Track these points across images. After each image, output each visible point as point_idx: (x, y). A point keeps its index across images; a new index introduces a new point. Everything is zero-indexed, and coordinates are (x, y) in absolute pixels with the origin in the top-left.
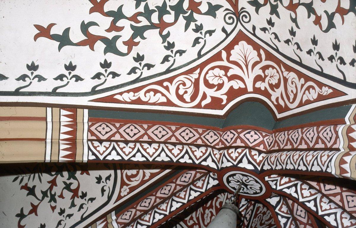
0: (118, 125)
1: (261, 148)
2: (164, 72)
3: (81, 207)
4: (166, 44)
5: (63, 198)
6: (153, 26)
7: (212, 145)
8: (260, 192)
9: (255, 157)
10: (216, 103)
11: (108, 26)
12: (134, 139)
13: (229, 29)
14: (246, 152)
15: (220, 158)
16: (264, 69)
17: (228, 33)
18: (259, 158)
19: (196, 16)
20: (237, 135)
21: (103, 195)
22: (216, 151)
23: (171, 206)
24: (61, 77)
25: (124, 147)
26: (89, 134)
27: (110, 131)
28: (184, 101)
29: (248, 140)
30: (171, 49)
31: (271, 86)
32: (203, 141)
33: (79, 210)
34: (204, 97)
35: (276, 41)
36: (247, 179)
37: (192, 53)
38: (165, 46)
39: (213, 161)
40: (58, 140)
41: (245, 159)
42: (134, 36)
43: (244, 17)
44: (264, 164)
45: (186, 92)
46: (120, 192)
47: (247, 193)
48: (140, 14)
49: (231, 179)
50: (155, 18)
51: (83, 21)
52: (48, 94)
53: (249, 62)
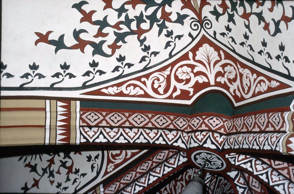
0: (104, 114)
1: (222, 131)
3: (75, 181)
4: (143, 47)
5: (60, 174)
6: (132, 32)
7: (182, 129)
9: (217, 139)
10: (185, 95)
11: (95, 33)
13: (194, 34)
15: (188, 140)
16: (224, 66)
17: (194, 37)
18: (220, 140)
19: (167, 23)
21: (92, 171)
22: (185, 134)
24: (57, 75)
25: (110, 132)
26: (81, 121)
29: (211, 124)
30: (147, 51)
31: (229, 80)
32: (174, 126)
34: (175, 89)
35: (233, 44)
37: (164, 54)
38: (142, 49)
41: (209, 140)
42: (116, 41)
43: (206, 25)
44: (224, 145)
45: (160, 86)
46: (107, 168)
47: (211, 168)
48: (121, 23)
49: (197, 157)
50: (134, 26)
51: (75, 29)
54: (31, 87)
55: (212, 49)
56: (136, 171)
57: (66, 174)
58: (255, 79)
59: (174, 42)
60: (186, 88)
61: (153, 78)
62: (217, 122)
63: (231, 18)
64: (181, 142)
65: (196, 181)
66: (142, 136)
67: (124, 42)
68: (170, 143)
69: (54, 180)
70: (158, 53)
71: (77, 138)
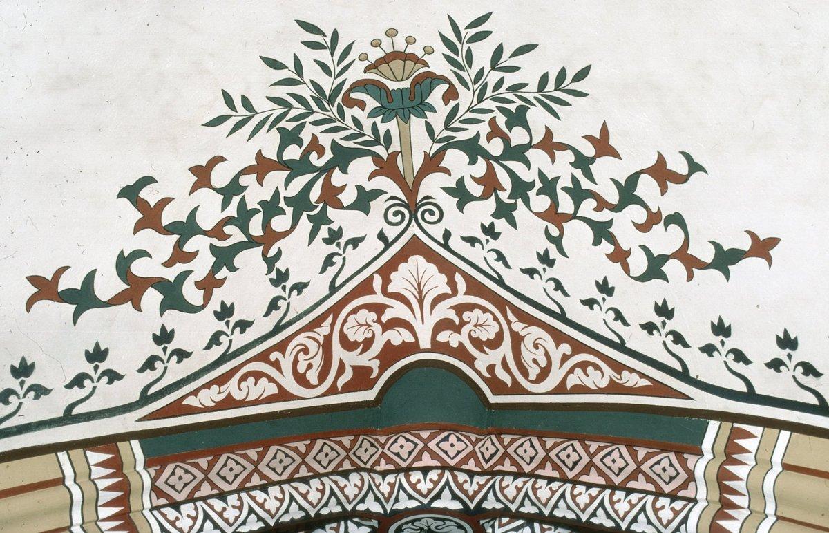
1: (471, 466)
4: (273, 275)
6: (252, 242)
7: (368, 466)
9: (466, 486)
10: (362, 378)
11: (167, 254)
13: (391, 233)
14: (448, 479)
15: (391, 494)
16: (460, 309)
17: (390, 241)
19: (331, 212)
24: (78, 381)
29: (446, 452)
32: (353, 463)
37: (319, 287)
38: (271, 280)
39: (377, 499)
42: (215, 269)
45: (310, 366)
48: (229, 221)
51: (122, 252)
53: (426, 294)
54: (17, 425)
55: (433, 268)
58: (564, 354)
59: (343, 256)
61: (294, 348)
63: (504, 211)
66: (294, 503)
67: (233, 269)
68: (349, 508)
70: (305, 285)
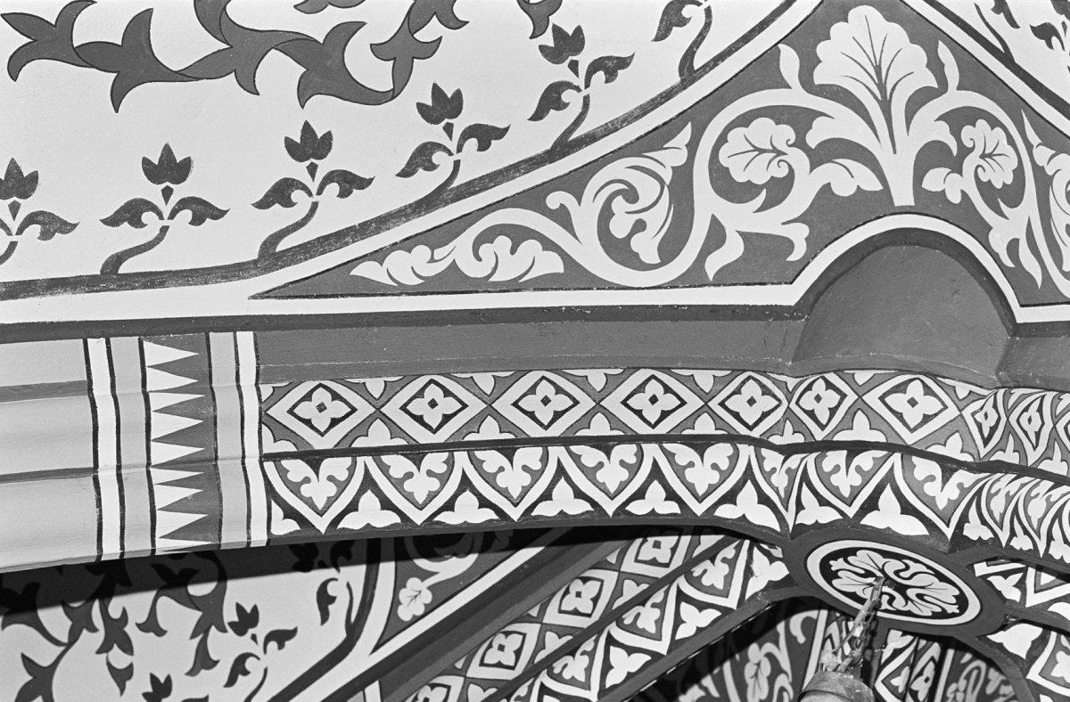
0: (376, 386)
1: (953, 449)
2: (547, 152)
3: (239, 668)
4: (548, 39)
5: (160, 632)
7: (756, 433)
8: (957, 611)
9: (931, 489)
10: (765, 258)
12: (441, 437)
16: (959, 119)
18: (944, 494)
20: (851, 397)
21: (325, 617)
22: (772, 459)
23: (607, 667)
24: (132, 213)
25: (409, 475)
27: (347, 415)
28: (629, 259)
29: (899, 416)
30: (570, 58)
31: (985, 188)
33: (231, 682)
34: (716, 236)
35: (999, 21)
36: (904, 567)
37: (656, 67)
38: (542, 48)
39: (764, 499)
40: (144, 469)
41: (888, 497)
44: (964, 519)
45: (640, 226)
46: (395, 603)
47: (909, 614)
49: (836, 565)
52: (88, 286)
53: (893, 89)
56: (538, 620)
57: (193, 636)
60: (771, 222)
62: (929, 405)
64: (756, 498)
65: (833, 693)
69: (131, 666)
71: (252, 520)
